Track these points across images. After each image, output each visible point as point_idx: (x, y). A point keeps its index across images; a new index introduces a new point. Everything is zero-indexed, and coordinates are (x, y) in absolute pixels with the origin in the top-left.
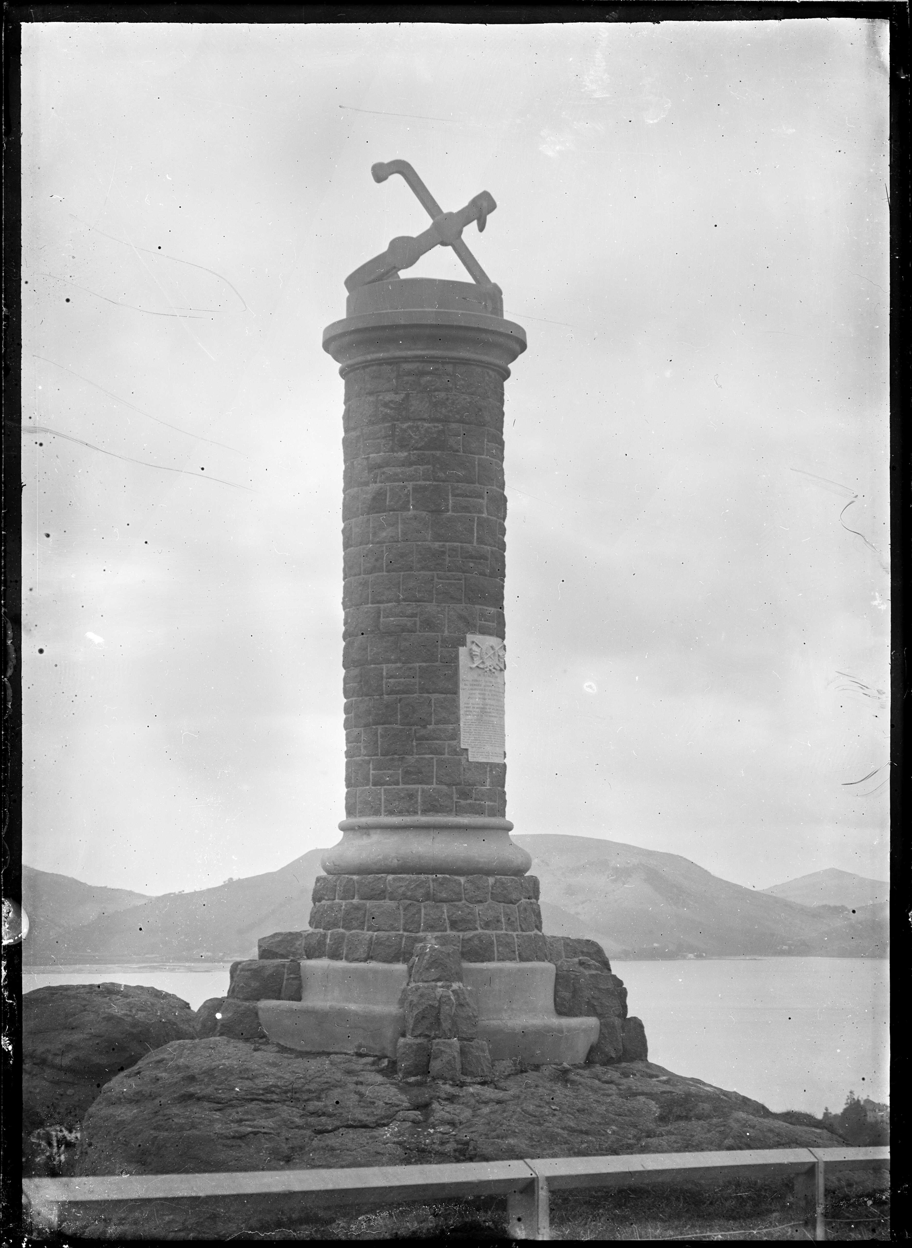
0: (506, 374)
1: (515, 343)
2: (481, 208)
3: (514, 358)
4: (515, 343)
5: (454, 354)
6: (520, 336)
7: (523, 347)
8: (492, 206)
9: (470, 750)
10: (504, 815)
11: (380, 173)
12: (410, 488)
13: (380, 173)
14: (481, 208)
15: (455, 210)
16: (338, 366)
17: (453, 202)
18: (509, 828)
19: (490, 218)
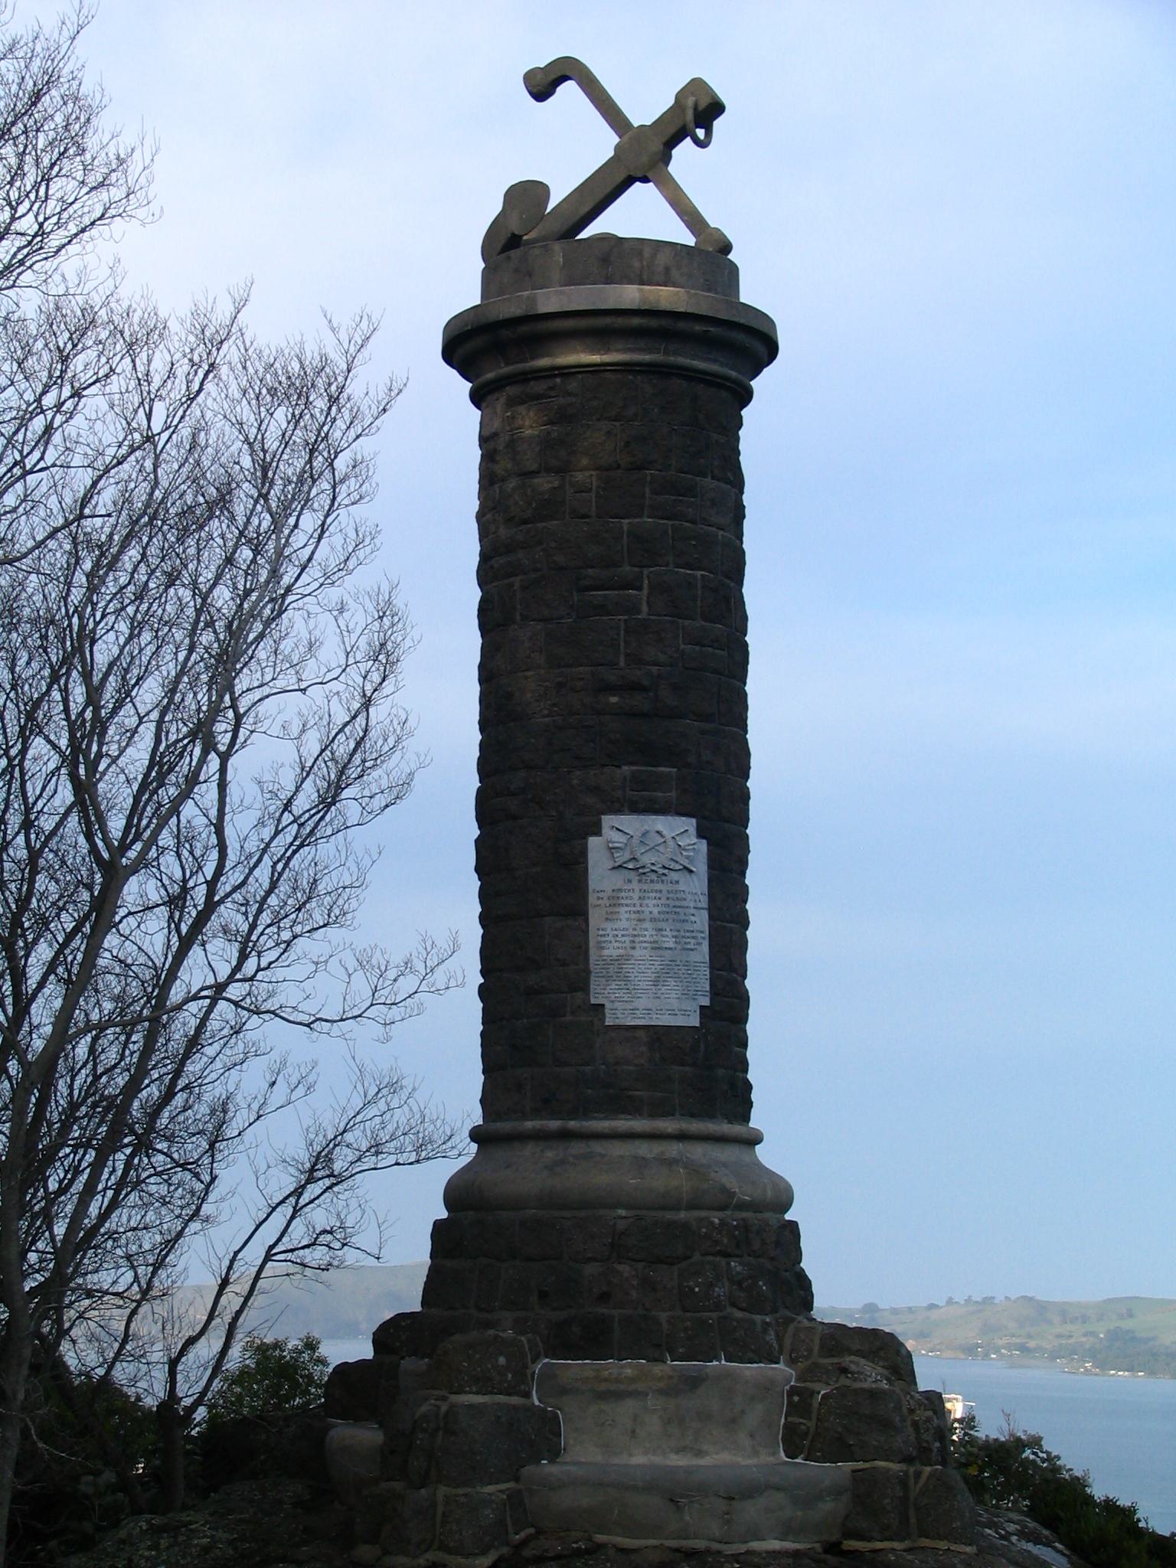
0: (745, 397)
1: (756, 343)
2: (698, 113)
3: (756, 372)
4: (756, 343)
5: (682, 360)
6: (765, 329)
7: (771, 350)
8: (716, 108)
9: (608, 1005)
10: (746, 1118)
11: (542, 85)
12: (517, 586)
13: (542, 85)
14: (698, 113)
15: (648, 122)
16: (468, 386)
17: (645, 108)
18: (755, 1139)
19: (717, 124)
